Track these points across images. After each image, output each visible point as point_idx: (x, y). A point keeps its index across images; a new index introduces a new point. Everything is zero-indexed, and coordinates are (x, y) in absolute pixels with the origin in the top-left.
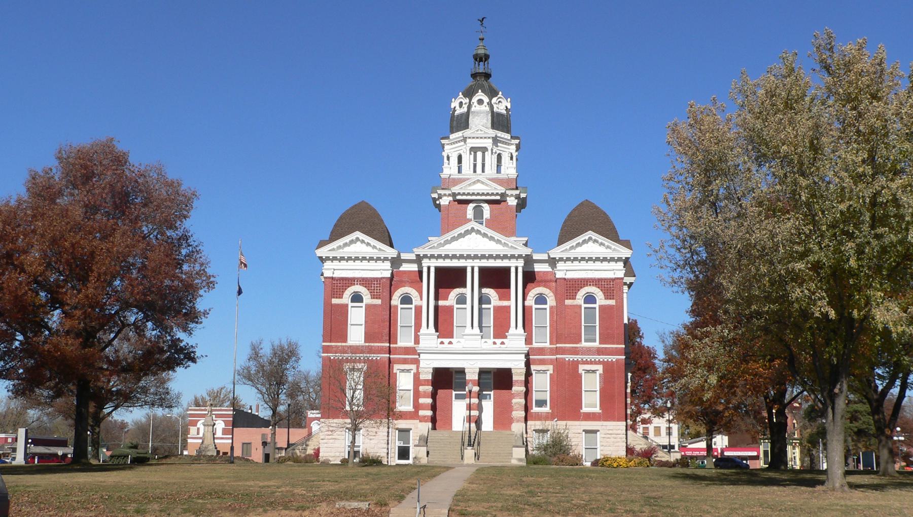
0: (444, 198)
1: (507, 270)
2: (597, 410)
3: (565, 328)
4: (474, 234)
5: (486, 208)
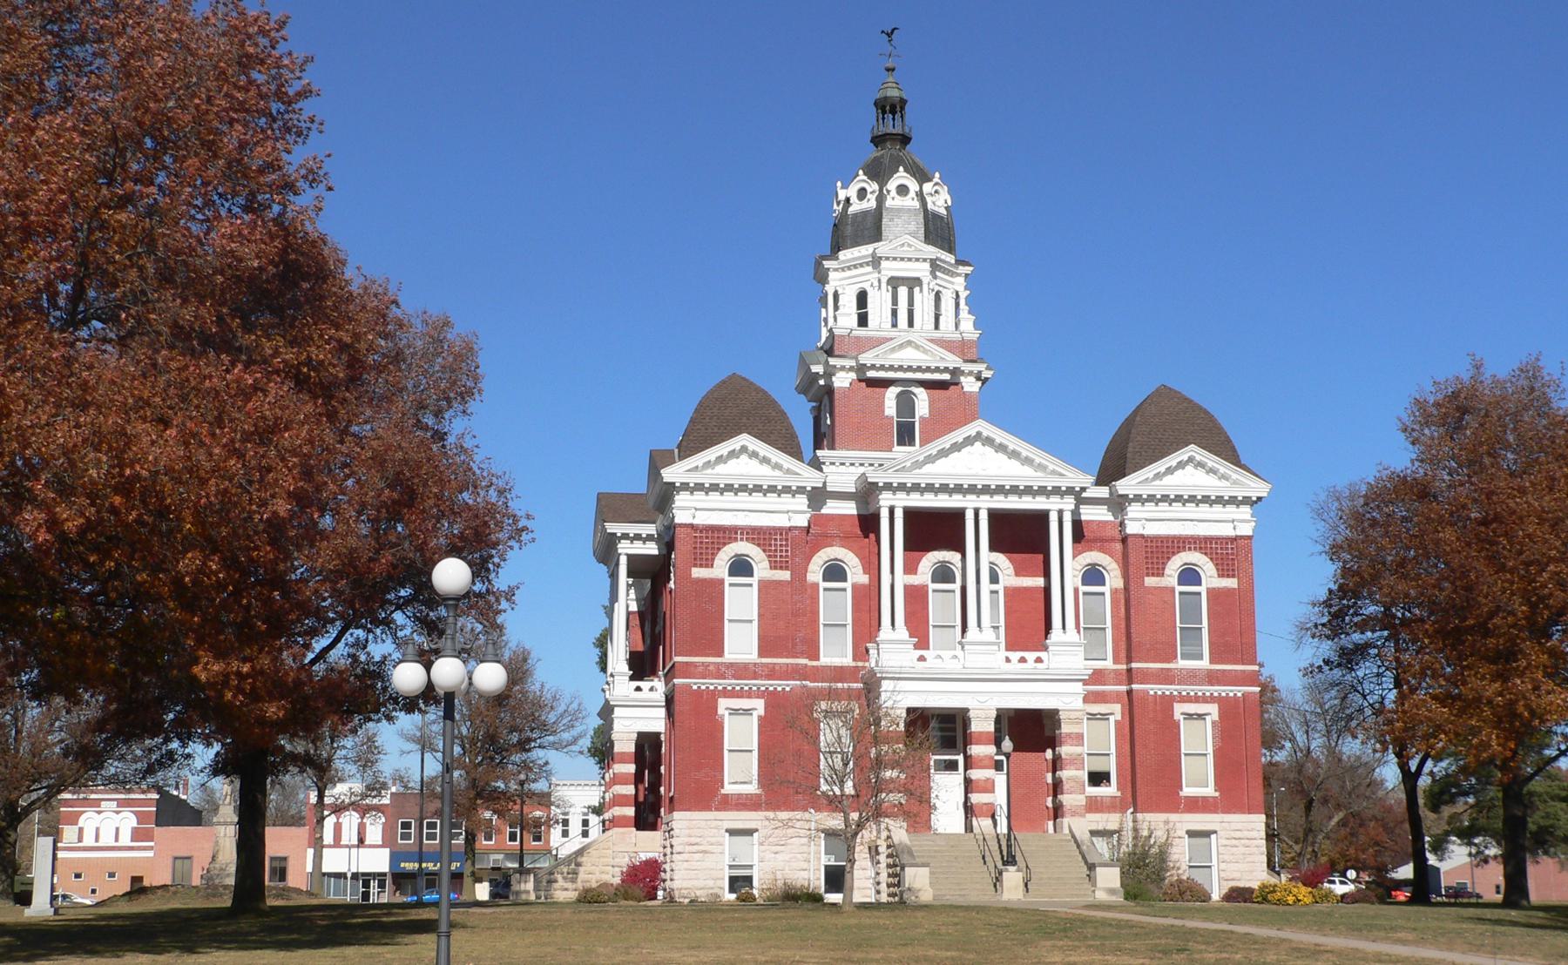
0: (841, 374)
1: (1041, 518)
2: (1210, 791)
3: (1138, 632)
5: (922, 399)
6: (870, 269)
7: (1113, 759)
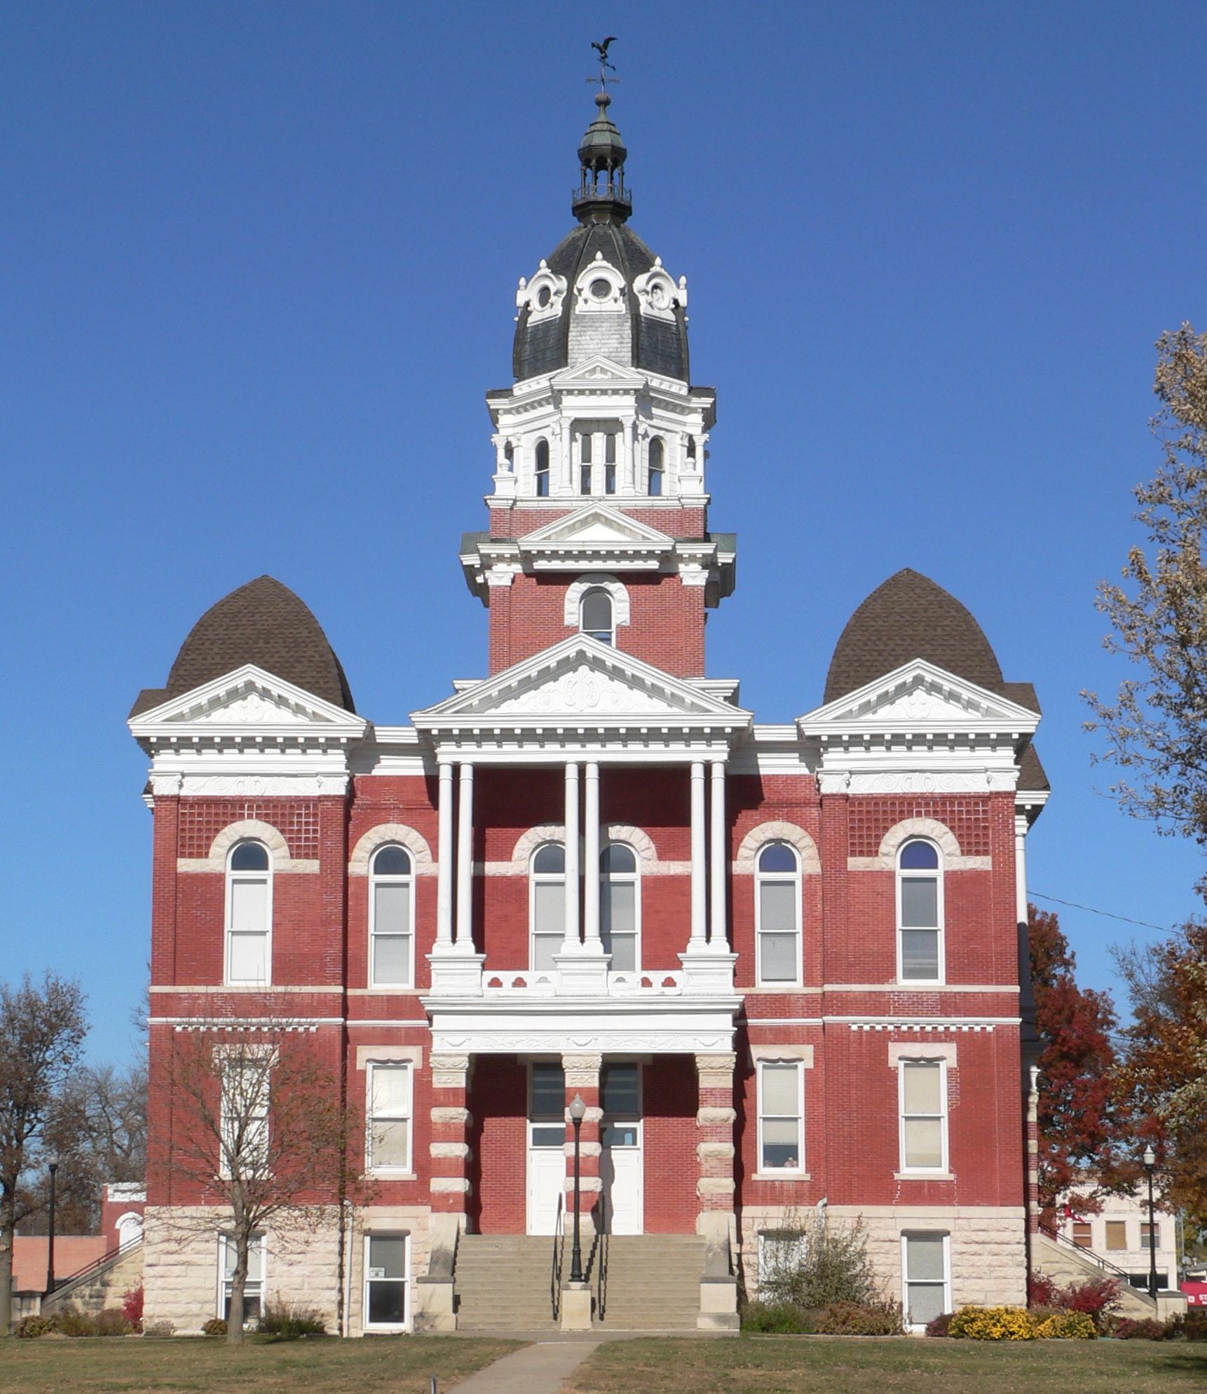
0: (500, 567)
1: (681, 772)
2: (942, 1172)
3: (848, 939)
4: (584, 669)
5: (619, 595)
6: (550, 408)
7: (801, 1125)
